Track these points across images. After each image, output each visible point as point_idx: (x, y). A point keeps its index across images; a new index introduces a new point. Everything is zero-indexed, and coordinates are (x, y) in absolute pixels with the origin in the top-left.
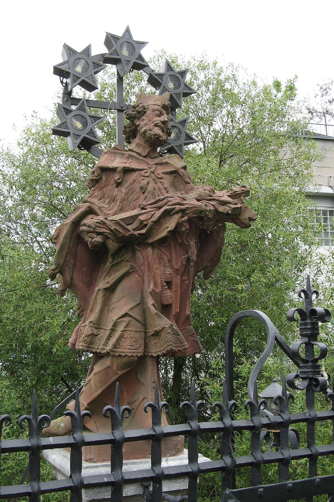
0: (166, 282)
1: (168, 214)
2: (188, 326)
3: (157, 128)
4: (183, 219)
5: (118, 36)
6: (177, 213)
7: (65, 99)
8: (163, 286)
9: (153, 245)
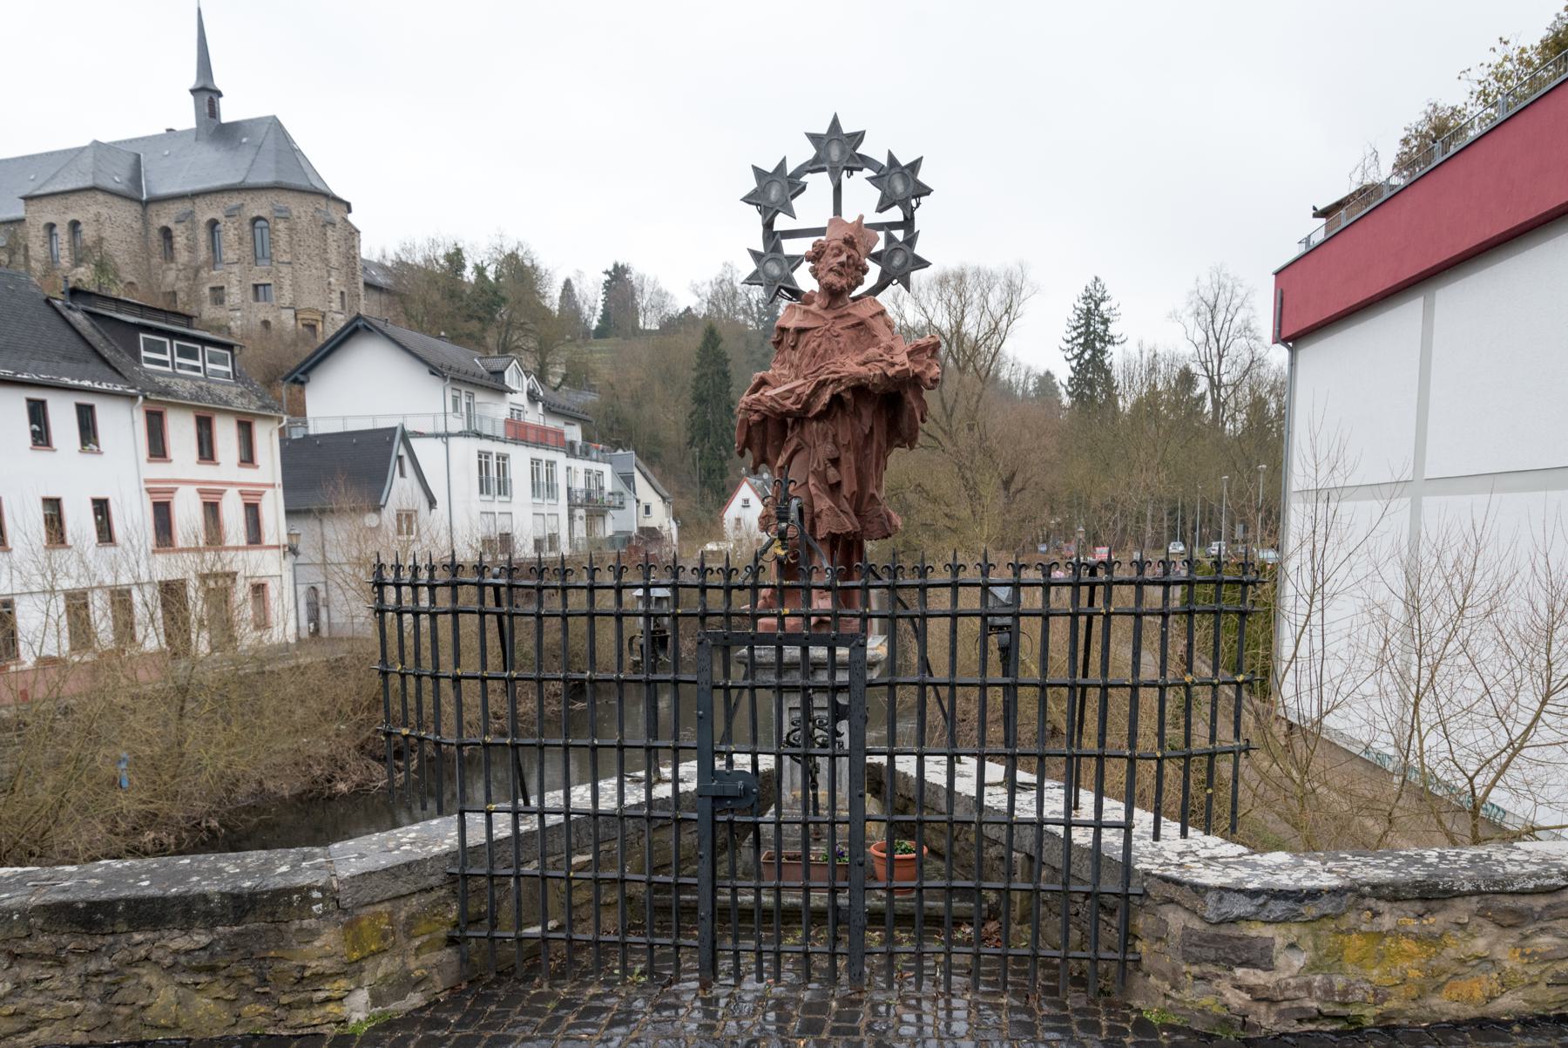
3: (831, 274)
9: (819, 417)
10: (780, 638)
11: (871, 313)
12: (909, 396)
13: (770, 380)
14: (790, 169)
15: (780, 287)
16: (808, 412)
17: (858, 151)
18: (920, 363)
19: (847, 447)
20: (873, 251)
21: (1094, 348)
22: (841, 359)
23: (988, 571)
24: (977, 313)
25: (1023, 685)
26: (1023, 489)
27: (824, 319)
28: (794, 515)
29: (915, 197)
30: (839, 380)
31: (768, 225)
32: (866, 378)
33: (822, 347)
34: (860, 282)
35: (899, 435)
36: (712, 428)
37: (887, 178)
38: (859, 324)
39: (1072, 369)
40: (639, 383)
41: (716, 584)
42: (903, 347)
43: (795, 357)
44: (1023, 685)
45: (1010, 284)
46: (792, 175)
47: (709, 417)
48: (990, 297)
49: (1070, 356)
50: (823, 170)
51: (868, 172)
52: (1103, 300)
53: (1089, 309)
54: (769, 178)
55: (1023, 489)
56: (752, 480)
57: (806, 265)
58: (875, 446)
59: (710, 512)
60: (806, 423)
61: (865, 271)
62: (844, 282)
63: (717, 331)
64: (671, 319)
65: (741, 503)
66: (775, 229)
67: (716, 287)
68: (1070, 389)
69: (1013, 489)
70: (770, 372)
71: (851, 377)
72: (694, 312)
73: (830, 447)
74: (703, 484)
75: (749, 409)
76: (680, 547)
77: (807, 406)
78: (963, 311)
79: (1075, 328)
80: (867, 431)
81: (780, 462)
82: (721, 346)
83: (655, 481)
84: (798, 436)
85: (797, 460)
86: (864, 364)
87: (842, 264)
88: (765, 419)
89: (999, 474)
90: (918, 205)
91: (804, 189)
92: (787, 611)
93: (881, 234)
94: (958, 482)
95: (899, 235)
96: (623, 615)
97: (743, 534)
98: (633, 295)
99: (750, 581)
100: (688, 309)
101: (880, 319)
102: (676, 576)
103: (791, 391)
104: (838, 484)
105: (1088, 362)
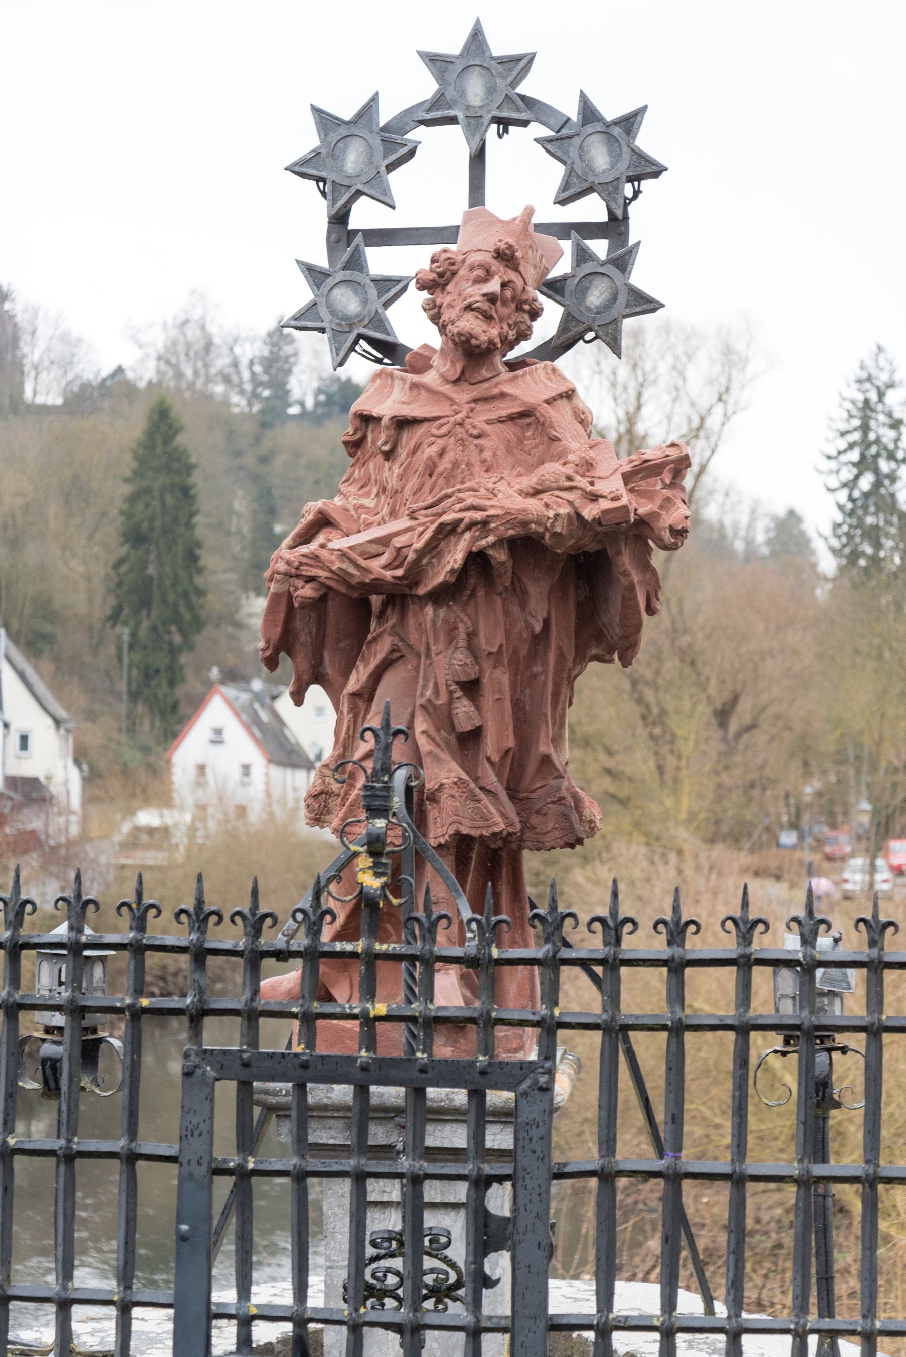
0: (457, 683)
1: (448, 531)
2: (554, 779)
3: (469, 316)
4: (483, 542)
5: (448, 56)
6: (469, 527)
7: (333, 236)
8: (451, 693)
9: (440, 596)
10: (364, 1068)
11: (547, 396)
12: (626, 560)
13: (337, 516)
14: (385, 116)
15: (360, 336)
16: (417, 584)
17: (522, 89)
18: (649, 495)
19: (496, 657)
20: (551, 276)
21: (876, 471)
22: (487, 481)
23: (815, 933)
24: (666, 398)
25: (890, 1180)
26: (752, 727)
27: (452, 401)
28: (397, 801)
29: (630, 179)
30: (485, 523)
31: (339, 219)
32: (538, 523)
33: (449, 457)
34: (524, 336)
35: (599, 637)
36: (156, 592)
37: (577, 141)
38: (523, 415)
39: (841, 507)
40: (20, 501)
41: (228, 945)
42: (615, 463)
43: (391, 473)
44: (890, 1180)
45: (728, 351)
46: (385, 129)
47: (152, 570)
48: (691, 372)
49: (834, 482)
50: (453, 120)
51: (538, 130)
52: (891, 385)
53: (866, 402)
54: (343, 131)
55: (752, 727)
56: (230, 691)
57: (415, 298)
58: (552, 657)
59: (147, 750)
60: (412, 607)
61: (535, 314)
62: (494, 332)
63: (173, 413)
64: (85, 387)
65: (209, 735)
66: (351, 226)
67: (173, 332)
68: (836, 543)
69: (734, 726)
70: (338, 501)
71: (510, 519)
72: (130, 375)
73: (461, 657)
74: (134, 696)
75: (294, 574)
76: (85, 819)
77: (415, 574)
78: (639, 395)
79: (843, 434)
80: (538, 628)
81: (355, 682)
82: (180, 440)
83: (41, 687)
84: (393, 631)
85: (389, 682)
86: (536, 493)
87: (491, 298)
88: (326, 595)
89: (709, 697)
90: (636, 193)
91: (412, 153)
92: (380, 1009)
93: (566, 246)
94: (633, 710)
95: (599, 247)
96: (22, 1006)
97: (209, 794)
98: (15, 341)
99: (301, 942)
100: (120, 370)
101: (564, 406)
102: (140, 924)
103: (384, 541)
104: (476, 734)
105: (866, 495)
